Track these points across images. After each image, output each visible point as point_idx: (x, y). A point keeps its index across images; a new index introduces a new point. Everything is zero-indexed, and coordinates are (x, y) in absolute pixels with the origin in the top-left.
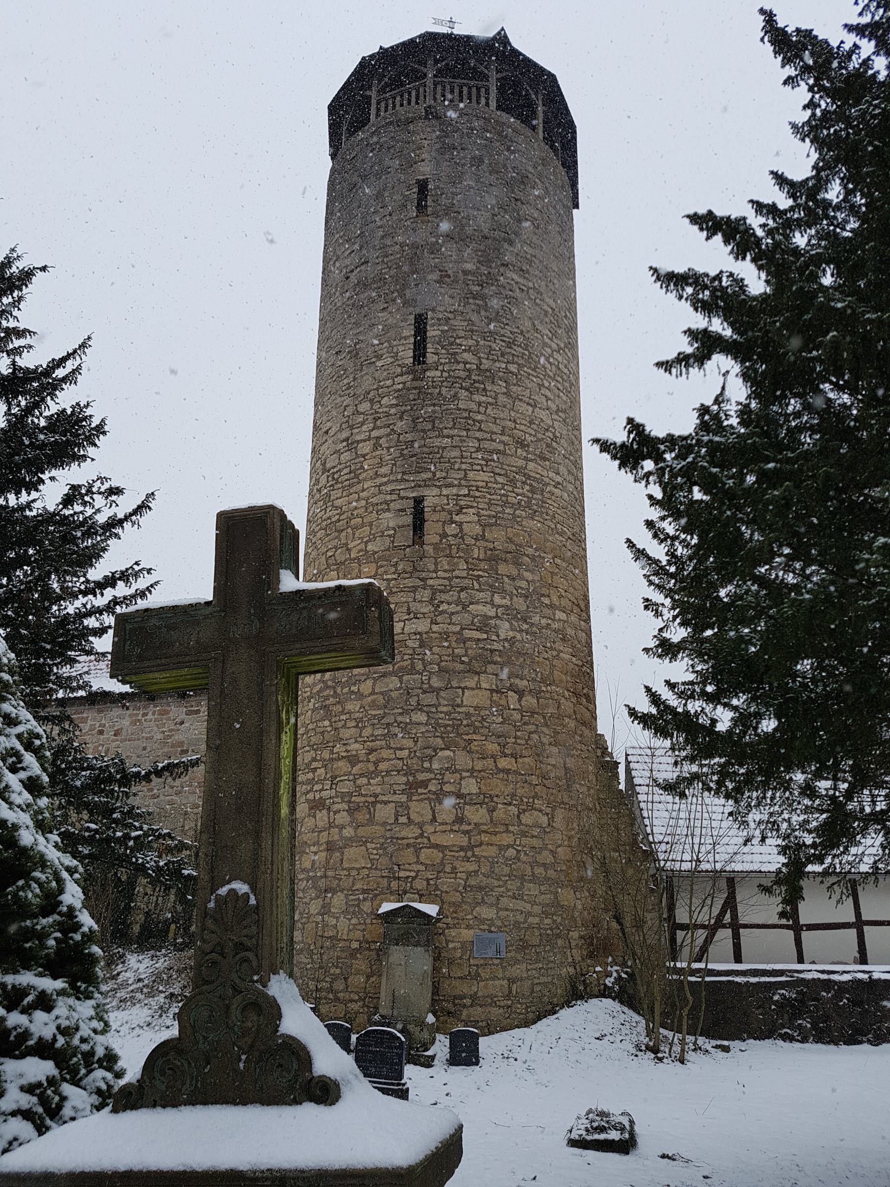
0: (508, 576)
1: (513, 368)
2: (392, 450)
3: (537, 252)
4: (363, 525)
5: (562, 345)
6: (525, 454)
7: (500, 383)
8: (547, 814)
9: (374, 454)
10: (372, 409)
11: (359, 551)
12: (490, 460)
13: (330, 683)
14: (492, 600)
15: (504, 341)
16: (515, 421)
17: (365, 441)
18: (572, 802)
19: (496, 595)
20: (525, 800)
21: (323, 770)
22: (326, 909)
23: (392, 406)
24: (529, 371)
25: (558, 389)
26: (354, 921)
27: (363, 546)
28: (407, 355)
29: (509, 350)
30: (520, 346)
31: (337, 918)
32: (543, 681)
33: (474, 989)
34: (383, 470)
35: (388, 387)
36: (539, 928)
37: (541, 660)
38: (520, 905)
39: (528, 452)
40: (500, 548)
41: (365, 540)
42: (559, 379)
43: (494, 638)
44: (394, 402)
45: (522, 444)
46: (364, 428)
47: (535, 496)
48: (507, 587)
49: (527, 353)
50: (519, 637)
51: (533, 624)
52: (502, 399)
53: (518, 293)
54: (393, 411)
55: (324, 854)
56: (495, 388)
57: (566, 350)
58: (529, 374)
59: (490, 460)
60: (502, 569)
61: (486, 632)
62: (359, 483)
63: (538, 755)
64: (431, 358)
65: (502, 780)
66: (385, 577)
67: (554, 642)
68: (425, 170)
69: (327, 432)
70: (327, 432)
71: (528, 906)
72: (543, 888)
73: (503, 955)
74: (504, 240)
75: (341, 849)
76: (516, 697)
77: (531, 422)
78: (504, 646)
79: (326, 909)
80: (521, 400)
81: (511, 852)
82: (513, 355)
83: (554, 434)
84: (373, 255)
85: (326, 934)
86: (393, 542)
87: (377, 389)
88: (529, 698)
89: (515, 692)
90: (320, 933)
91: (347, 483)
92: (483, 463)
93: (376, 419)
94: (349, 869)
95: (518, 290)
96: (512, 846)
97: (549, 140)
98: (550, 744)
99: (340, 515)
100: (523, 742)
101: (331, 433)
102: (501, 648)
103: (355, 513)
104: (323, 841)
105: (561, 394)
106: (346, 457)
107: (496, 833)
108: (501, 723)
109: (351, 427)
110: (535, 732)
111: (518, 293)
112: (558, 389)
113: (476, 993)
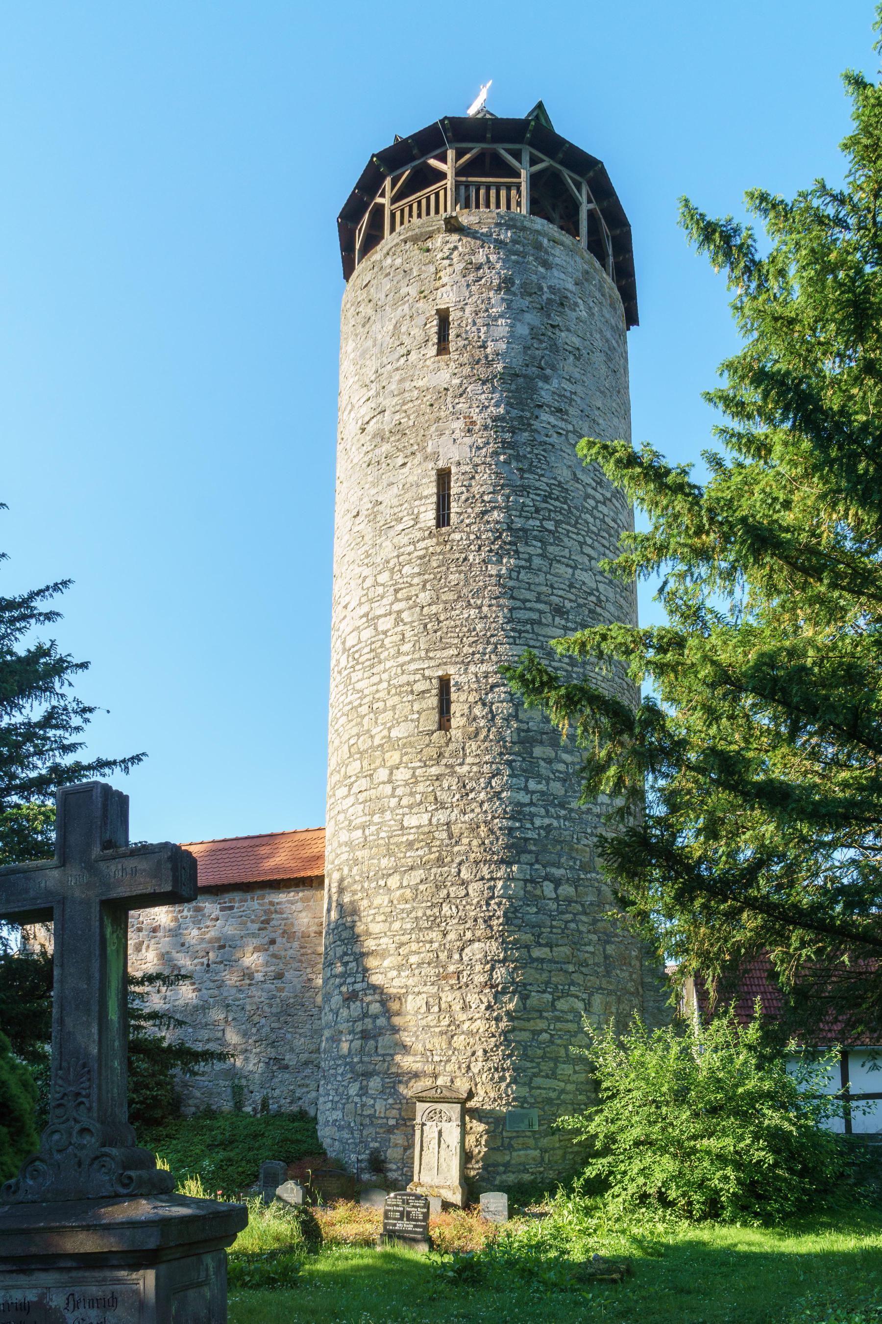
0: (543, 759)
1: (550, 525)
2: (415, 624)
3: (579, 389)
4: (385, 710)
5: (608, 495)
6: (563, 622)
7: (534, 543)
8: (584, 1000)
9: (396, 629)
10: (392, 579)
11: (384, 737)
12: (524, 631)
13: (357, 878)
14: (526, 786)
15: (539, 495)
16: (552, 587)
17: (385, 615)
18: (611, 987)
19: (530, 780)
20: (560, 987)
21: (354, 964)
22: (363, 1091)
23: (413, 576)
24: (569, 527)
25: (604, 546)
26: (391, 1101)
27: (385, 732)
28: (429, 517)
29: (544, 505)
30: (557, 499)
31: (375, 1099)
32: (583, 868)
33: (507, 1158)
34: (407, 647)
35: (409, 554)
36: (572, 1104)
37: (580, 847)
38: (553, 1083)
39: (567, 620)
40: (535, 728)
41: (388, 725)
42: (605, 535)
43: (529, 826)
44: (416, 570)
45: (559, 611)
46: (385, 601)
47: (575, 669)
48: (543, 771)
49: (565, 507)
50: (555, 823)
51: (571, 810)
52: (537, 561)
53: (555, 439)
54: (416, 580)
55: (359, 1042)
56: (530, 550)
57: (614, 500)
58: (568, 531)
59: (524, 631)
60: (538, 751)
61: (520, 820)
62: (380, 662)
63: (574, 943)
64: (454, 518)
65: (536, 969)
66: (410, 765)
67: (596, 828)
68: (447, 298)
69: (345, 607)
70: (345, 607)
71: (562, 1084)
72: (577, 1068)
73: (536, 1128)
74: (538, 377)
75: (375, 1037)
76: (552, 886)
77: (571, 586)
78: (539, 834)
79: (363, 1091)
80: (559, 562)
81: (545, 1036)
82: (550, 511)
83: (598, 597)
84: (389, 402)
85: (365, 1113)
86: (418, 727)
87: (398, 556)
88: (566, 886)
89: (551, 881)
90: (359, 1112)
91: (368, 663)
92: (517, 635)
93: (396, 591)
94: (383, 1055)
95: (555, 435)
96: (546, 1031)
97: (596, 247)
98: (589, 932)
99: (361, 698)
100: (559, 931)
101: (350, 607)
102: (536, 837)
103: (377, 696)
104: (359, 1029)
105: (607, 552)
106: (367, 634)
107: (529, 1020)
108: (536, 913)
109: (371, 601)
110: (572, 921)
111: (555, 439)
112: (604, 546)
113: (509, 1162)
